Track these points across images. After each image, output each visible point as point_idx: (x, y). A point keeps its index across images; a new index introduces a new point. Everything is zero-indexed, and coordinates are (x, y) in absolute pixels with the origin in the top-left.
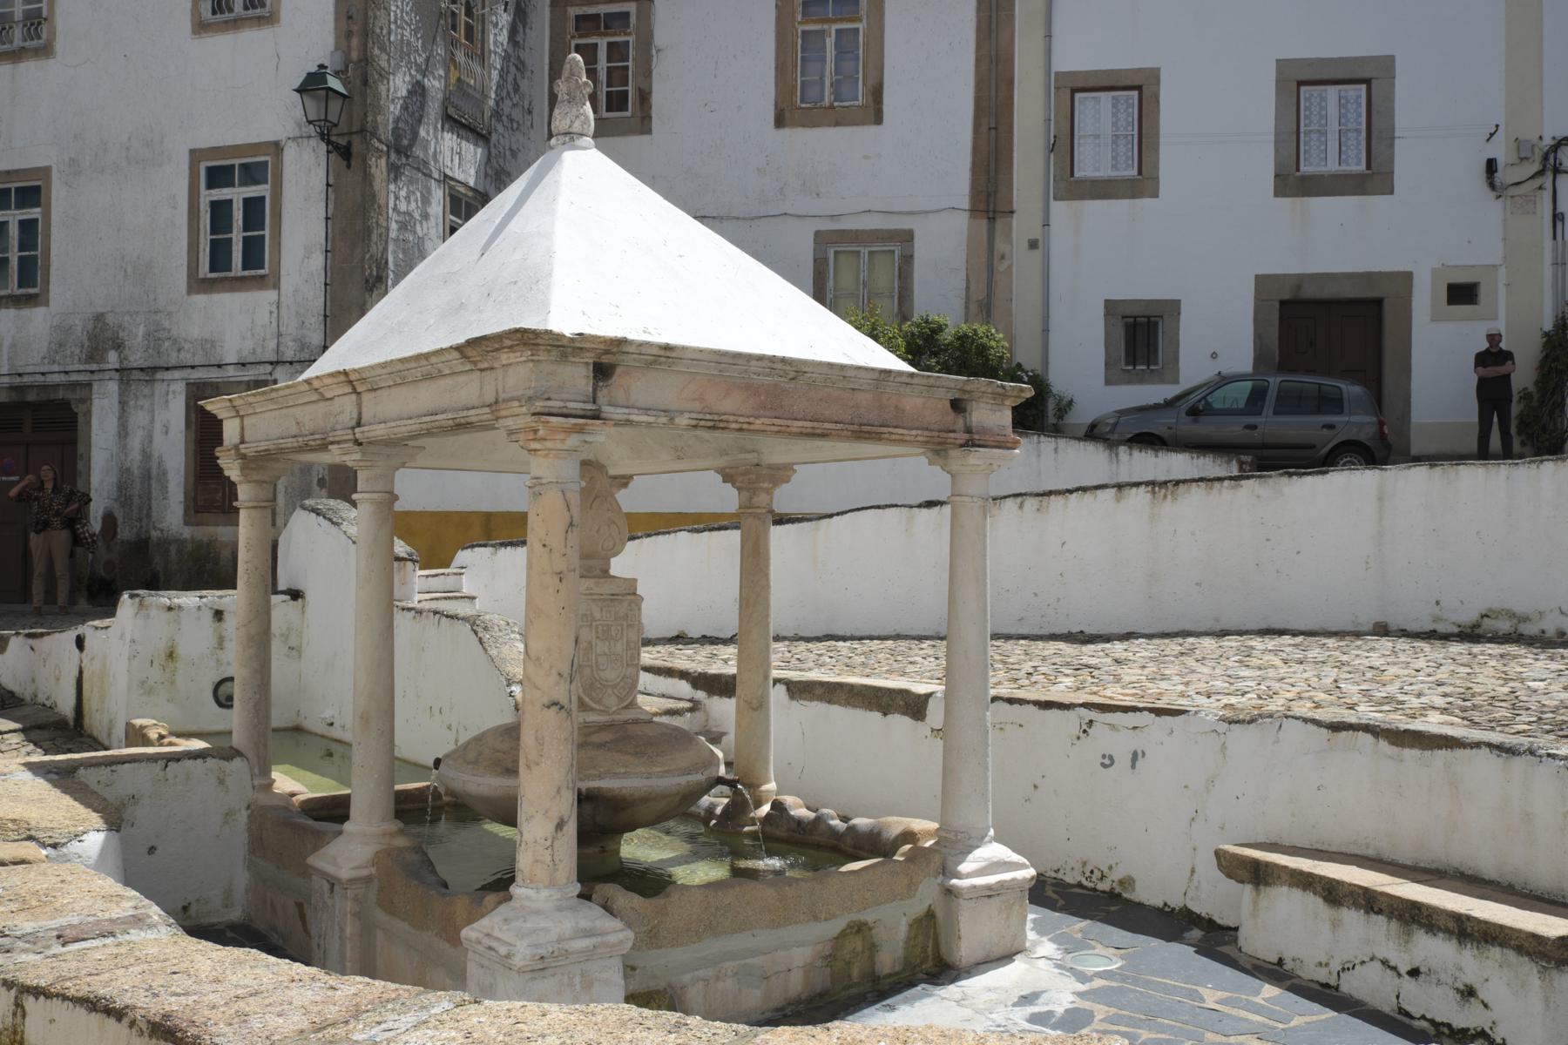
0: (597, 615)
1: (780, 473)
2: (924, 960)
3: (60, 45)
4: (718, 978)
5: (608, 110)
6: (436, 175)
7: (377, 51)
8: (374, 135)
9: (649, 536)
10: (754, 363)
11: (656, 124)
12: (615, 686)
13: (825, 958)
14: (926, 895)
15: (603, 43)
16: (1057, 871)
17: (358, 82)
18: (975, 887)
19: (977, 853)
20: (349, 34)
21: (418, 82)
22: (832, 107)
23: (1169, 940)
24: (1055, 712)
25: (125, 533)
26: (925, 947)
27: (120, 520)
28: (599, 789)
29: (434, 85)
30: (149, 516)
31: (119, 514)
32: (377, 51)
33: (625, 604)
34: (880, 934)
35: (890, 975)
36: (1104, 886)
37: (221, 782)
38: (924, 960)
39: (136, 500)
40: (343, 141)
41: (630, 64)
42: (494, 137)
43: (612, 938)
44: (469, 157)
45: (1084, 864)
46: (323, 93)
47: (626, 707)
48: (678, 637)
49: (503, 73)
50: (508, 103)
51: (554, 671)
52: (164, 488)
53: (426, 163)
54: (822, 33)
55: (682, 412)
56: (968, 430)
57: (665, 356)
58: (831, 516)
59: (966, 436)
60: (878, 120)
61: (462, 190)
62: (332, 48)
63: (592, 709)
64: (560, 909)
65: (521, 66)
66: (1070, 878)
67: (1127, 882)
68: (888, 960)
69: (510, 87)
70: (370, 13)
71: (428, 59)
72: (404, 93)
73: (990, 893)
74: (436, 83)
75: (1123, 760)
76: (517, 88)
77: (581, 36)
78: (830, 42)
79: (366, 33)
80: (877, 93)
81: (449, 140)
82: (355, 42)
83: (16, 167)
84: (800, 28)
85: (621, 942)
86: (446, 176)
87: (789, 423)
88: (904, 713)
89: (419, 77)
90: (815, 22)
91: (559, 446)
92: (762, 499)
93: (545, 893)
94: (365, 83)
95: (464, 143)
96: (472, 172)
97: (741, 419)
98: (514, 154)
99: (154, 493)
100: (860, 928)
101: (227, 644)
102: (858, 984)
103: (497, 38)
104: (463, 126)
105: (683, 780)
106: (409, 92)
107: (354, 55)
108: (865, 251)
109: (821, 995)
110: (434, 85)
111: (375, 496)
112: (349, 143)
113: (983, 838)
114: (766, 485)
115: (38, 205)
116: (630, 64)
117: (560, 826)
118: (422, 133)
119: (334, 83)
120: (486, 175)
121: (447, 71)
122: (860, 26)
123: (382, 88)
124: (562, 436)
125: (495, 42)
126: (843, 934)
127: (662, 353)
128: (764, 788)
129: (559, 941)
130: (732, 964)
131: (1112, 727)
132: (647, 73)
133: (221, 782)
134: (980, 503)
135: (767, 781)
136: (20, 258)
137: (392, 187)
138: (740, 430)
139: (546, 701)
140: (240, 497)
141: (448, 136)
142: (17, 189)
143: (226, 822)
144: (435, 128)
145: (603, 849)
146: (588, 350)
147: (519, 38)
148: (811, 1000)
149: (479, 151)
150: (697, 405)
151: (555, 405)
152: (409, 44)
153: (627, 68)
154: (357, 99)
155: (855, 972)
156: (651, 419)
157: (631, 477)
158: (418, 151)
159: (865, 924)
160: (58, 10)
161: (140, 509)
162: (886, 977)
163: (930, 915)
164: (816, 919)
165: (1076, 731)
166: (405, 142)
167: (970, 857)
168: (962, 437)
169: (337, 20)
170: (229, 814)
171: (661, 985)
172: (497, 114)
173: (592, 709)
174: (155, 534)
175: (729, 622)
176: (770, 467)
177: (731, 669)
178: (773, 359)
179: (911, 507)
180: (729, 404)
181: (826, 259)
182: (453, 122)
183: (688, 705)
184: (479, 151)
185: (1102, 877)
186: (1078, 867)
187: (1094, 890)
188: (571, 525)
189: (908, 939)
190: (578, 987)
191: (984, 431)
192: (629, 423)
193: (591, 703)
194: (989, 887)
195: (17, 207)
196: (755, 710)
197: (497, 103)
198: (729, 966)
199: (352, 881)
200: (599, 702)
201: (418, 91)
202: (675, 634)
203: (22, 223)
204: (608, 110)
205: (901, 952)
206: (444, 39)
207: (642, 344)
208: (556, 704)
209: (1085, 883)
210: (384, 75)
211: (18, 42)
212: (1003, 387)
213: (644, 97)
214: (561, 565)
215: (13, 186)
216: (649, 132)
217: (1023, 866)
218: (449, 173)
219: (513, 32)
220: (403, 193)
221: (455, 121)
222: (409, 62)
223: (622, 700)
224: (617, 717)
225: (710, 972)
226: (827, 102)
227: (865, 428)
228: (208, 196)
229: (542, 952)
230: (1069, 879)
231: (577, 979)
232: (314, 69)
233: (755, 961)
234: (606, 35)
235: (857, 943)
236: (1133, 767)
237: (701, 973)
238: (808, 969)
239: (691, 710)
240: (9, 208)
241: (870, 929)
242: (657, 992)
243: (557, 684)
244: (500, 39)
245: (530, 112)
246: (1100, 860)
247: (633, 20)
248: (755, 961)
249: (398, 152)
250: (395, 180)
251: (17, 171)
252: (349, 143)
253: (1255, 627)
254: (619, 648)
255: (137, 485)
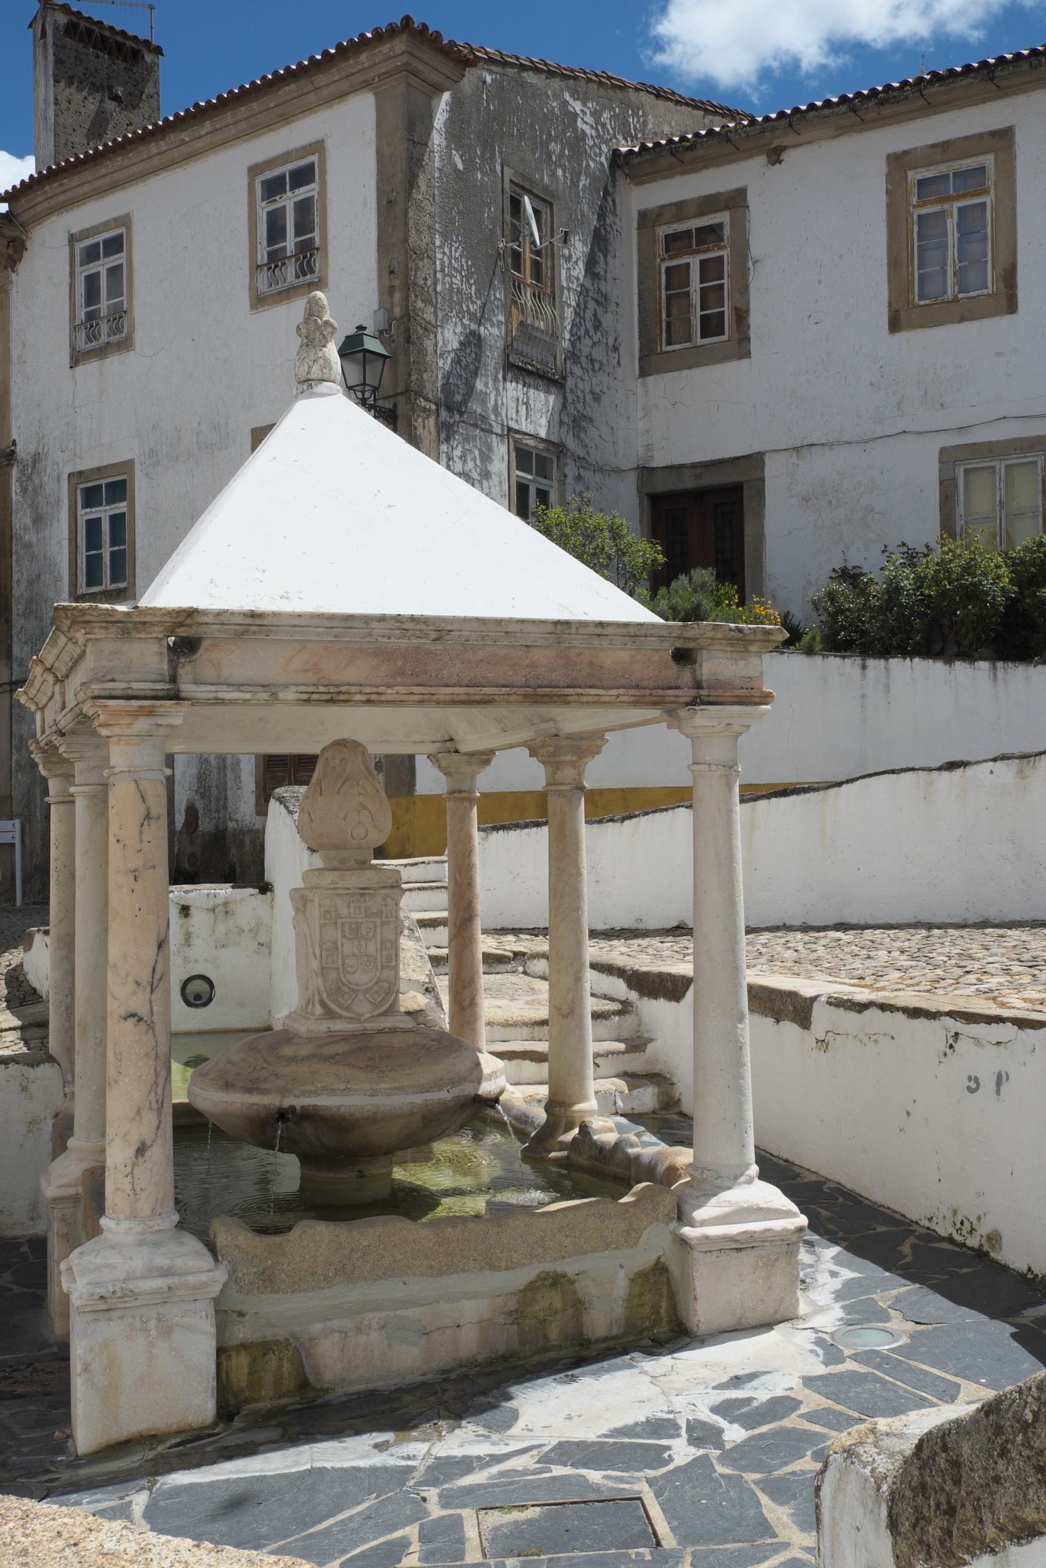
0: (343, 910)
1: (587, 745)
2: (656, 1323)
3: (138, 337)
4: (359, 1331)
5: (703, 336)
6: (498, 430)
7: (420, 304)
8: (419, 394)
9: (646, 814)
10: (374, 624)
11: (755, 346)
12: (367, 991)
13: (509, 1314)
14: (652, 1245)
15: (694, 262)
16: (930, 1219)
17: (401, 339)
18: (707, 1237)
19: (724, 1196)
20: (392, 290)
21: (472, 333)
22: (956, 300)
23: (993, 1316)
24: (922, 1022)
25: (205, 825)
26: (656, 1309)
27: (201, 812)
28: (315, 1107)
29: (493, 333)
30: (225, 807)
31: (199, 806)
32: (420, 304)
33: (379, 899)
34: (586, 1288)
35: (606, 1339)
36: (973, 1242)
37: (24, 1089)
38: (656, 1323)
39: (214, 790)
40: (388, 405)
41: (725, 281)
42: (570, 382)
43: (192, 1280)
44: (539, 406)
45: (955, 1212)
46: (361, 355)
47: (384, 1014)
48: (678, 927)
49: (579, 312)
50: (587, 342)
51: (130, 979)
52: (238, 778)
53: (484, 418)
54: (941, 215)
55: (286, 686)
56: (698, 686)
57: (254, 625)
58: (839, 784)
59: (693, 692)
60: (1011, 306)
61: (531, 442)
62: (376, 306)
63: (341, 1017)
64: (140, 1244)
65: (603, 300)
66: (944, 1229)
67: (994, 1238)
68: (601, 1320)
69: (589, 325)
70: (411, 265)
71: (484, 306)
72: (456, 345)
73: (738, 1246)
74: (495, 331)
75: (988, 1084)
76: (598, 324)
77: (671, 258)
78: (952, 224)
79: (408, 286)
80: (1009, 278)
81: (513, 390)
82: (397, 297)
83: (111, 462)
84: (916, 213)
85: (204, 1285)
86: (510, 429)
87: (433, 690)
88: (793, 1020)
89: (473, 327)
90: (932, 203)
91: (127, 731)
92: (567, 774)
93: (125, 1225)
94: (408, 340)
95: (532, 392)
96: (544, 422)
97: (367, 690)
98: (596, 397)
99: (229, 783)
100: (556, 1281)
101: (194, 940)
102: (559, 1347)
103: (571, 269)
104: (530, 373)
105: (418, 1099)
106: (461, 343)
107: (397, 312)
108: (1001, 466)
109: (505, 1358)
110: (493, 333)
111: (87, 789)
112: (395, 405)
113: (736, 1178)
114: (568, 758)
115: (124, 499)
116: (725, 281)
117: (141, 1150)
118: (479, 385)
119: (372, 344)
120: (561, 423)
121: (509, 316)
122: (988, 199)
123: (428, 344)
124: (127, 720)
125: (569, 278)
126: (532, 1287)
127: (249, 621)
128: (577, 1107)
129: (125, 1280)
130: (378, 1315)
131: (977, 1041)
132: (743, 289)
133: (24, 1089)
134: (721, 771)
135: (583, 1098)
136: (112, 553)
137: (444, 447)
138: (369, 702)
139: (122, 1011)
140: (51, 792)
141: (511, 386)
142: (107, 484)
143: (30, 1131)
144: (496, 379)
145: (361, 1174)
146: (153, 624)
147: (599, 269)
148: (491, 1362)
149: (552, 398)
150: (310, 677)
151: (118, 686)
152: (460, 291)
153: (722, 286)
154: (401, 358)
155: (554, 1333)
156: (248, 696)
157: (492, 752)
158: (475, 406)
159: (564, 1276)
160: (136, 301)
161: (218, 800)
162: (598, 1341)
163: (660, 1269)
164: (492, 1267)
165: (942, 1046)
166: (458, 398)
167: (714, 1200)
168: (687, 694)
169: (380, 277)
170: (33, 1123)
171: (281, 1334)
172: (573, 356)
173: (341, 1017)
174: (231, 825)
175: (539, 912)
176: (570, 737)
177: (685, 968)
178: (398, 618)
179: (930, 770)
180: (355, 673)
181: (955, 480)
182: (517, 369)
183: (615, 1006)
184: (552, 398)
185: (972, 1230)
186: (949, 1215)
187: (964, 1245)
188: (148, 817)
189: (630, 1298)
190: (153, 1333)
191: (718, 684)
192: (220, 702)
193: (338, 1010)
194: (731, 1239)
195: (108, 503)
196: (564, 1017)
197: (573, 344)
198: (375, 1318)
199: (56, 1200)
200: (348, 1008)
201: (473, 342)
202: (675, 924)
203: (112, 517)
204: (703, 336)
205: (619, 1312)
206: (503, 281)
207: (219, 613)
208: (133, 1015)
209: (957, 1237)
210: (430, 329)
211: (104, 339)
212: (740, 630)
213: (742, 316)
214: (135, 862)
215: (103, 482)
216: (747, 354)
217: (788, 1214)
218: (513, 425)
219: (591, 263)
220: (457, 453)
221: (519, 368)
222: (461, 311)
223: (376, 1006)
224: (369, 1025)
225: (347, 1323)
226: (950, 295)
227: (540, 691)
228: (85, 515)
229: (102, 1291)
230: (942, 1231)
231: (152, 1324)
232: (352, 331)
233: (411, 1313)
234: (697, 252)
235: (555, 1298)
236: (998, 1092)
237: (336, 1323)
238: (485, 1326)
239: (619, 1013)
240: (101, 504)
241: (572, 1282)
242: (277, 1343)
243: (135, 993)
244: (574, 273)
245: (616, 349)
246: (969, 1210)
247: (727, 231)
248: (411, 1313)
249: (450, 409)
250: (447, 440)
251: (106, 467)
252: (395, 405)
253: (831, 923)
254: (372, 948)
255: (214, 775)
